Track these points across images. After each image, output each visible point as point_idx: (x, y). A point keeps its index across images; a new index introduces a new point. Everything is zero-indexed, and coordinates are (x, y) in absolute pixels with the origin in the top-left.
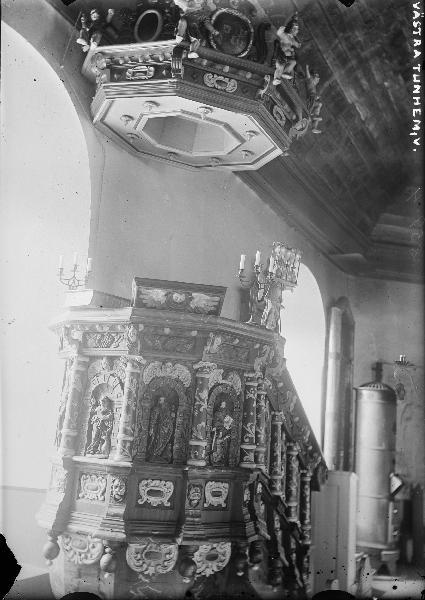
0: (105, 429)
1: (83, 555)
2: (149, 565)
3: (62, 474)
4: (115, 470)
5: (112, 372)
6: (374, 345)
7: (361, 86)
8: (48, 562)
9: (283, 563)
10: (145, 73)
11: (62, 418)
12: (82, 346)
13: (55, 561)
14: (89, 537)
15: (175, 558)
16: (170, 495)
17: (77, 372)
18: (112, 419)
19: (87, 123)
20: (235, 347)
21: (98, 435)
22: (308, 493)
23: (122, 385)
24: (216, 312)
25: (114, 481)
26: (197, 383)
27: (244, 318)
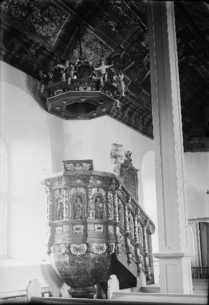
12: (50, 187)
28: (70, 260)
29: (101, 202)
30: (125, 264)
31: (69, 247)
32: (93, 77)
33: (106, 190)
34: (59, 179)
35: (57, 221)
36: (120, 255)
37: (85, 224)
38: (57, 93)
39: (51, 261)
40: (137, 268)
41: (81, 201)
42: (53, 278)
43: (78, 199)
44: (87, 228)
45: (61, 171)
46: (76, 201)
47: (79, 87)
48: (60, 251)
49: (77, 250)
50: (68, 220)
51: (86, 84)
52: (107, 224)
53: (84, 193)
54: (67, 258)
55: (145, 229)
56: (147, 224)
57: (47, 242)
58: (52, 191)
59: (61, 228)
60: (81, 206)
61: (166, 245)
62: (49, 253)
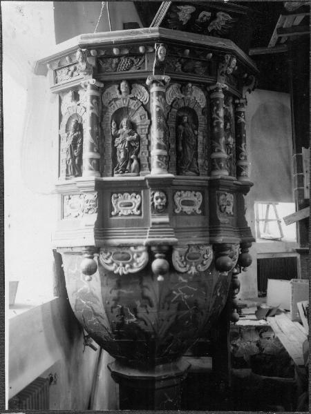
0: (136, 148)
1: (127, 266)
2: (191, 265)
5: (132, 96)
6: (154, 310)
8: (87, 277)
9: (238, 58)
11: (76, 144)
13: (93, 276)
14: (132, 248)
15: (212, 257)
16: (200, 203)
17: (93, 97)
20: (246, 72)
21: (127, 155)
25: (153, 194)
26: (161, 40)
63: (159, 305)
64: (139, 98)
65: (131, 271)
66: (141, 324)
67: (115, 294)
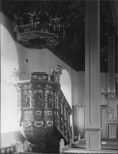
0: (28, 103)
3: (20, 112)
4: (31, 109)
7: (60, 57)
8: (20, 126)
10: (28, 30)
12: (21, 88)
18: (29, 101)
19: (16, 42)
22: (68, 115)
23: (30, 94)
24: (47, 79)
27: (51, 80)
28: (33, 129)
29: (51, 98)
30: (60, 131)
31: (33, 123)
32: (49, 24)
33: (54, 92)
34: (28, 84)
35: (25, 108)
36: (58, 126)
37: (43, 110)
38: (26, 31)
39: (22, 130)
40: (60, 128)
41: (40, 97)
42: (20, 138)
43: (39, 96)
44: (44, 112)
45: (29, 79)
46: (38, 97)
47: (41, 29)
48: (27, 124)
49: (38, 124)
50: (33, 108)
51: (45, 28)
52: (54, 110)
53: (42, 93)
54: (32, 128)
55: (68, 112)
56: (69, 109)
57: (20, 119)
58: (22, 91)
59: (28, 112)
60: (40, 100)
61: (90, 124)
62: (21, 125)
63: (33, 132)
64: (60, 69)
65: (28, 126)
66: (30, 135)
67: (25, 130)
